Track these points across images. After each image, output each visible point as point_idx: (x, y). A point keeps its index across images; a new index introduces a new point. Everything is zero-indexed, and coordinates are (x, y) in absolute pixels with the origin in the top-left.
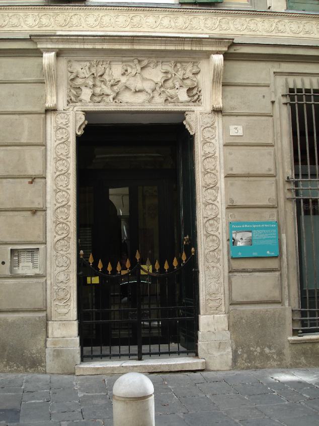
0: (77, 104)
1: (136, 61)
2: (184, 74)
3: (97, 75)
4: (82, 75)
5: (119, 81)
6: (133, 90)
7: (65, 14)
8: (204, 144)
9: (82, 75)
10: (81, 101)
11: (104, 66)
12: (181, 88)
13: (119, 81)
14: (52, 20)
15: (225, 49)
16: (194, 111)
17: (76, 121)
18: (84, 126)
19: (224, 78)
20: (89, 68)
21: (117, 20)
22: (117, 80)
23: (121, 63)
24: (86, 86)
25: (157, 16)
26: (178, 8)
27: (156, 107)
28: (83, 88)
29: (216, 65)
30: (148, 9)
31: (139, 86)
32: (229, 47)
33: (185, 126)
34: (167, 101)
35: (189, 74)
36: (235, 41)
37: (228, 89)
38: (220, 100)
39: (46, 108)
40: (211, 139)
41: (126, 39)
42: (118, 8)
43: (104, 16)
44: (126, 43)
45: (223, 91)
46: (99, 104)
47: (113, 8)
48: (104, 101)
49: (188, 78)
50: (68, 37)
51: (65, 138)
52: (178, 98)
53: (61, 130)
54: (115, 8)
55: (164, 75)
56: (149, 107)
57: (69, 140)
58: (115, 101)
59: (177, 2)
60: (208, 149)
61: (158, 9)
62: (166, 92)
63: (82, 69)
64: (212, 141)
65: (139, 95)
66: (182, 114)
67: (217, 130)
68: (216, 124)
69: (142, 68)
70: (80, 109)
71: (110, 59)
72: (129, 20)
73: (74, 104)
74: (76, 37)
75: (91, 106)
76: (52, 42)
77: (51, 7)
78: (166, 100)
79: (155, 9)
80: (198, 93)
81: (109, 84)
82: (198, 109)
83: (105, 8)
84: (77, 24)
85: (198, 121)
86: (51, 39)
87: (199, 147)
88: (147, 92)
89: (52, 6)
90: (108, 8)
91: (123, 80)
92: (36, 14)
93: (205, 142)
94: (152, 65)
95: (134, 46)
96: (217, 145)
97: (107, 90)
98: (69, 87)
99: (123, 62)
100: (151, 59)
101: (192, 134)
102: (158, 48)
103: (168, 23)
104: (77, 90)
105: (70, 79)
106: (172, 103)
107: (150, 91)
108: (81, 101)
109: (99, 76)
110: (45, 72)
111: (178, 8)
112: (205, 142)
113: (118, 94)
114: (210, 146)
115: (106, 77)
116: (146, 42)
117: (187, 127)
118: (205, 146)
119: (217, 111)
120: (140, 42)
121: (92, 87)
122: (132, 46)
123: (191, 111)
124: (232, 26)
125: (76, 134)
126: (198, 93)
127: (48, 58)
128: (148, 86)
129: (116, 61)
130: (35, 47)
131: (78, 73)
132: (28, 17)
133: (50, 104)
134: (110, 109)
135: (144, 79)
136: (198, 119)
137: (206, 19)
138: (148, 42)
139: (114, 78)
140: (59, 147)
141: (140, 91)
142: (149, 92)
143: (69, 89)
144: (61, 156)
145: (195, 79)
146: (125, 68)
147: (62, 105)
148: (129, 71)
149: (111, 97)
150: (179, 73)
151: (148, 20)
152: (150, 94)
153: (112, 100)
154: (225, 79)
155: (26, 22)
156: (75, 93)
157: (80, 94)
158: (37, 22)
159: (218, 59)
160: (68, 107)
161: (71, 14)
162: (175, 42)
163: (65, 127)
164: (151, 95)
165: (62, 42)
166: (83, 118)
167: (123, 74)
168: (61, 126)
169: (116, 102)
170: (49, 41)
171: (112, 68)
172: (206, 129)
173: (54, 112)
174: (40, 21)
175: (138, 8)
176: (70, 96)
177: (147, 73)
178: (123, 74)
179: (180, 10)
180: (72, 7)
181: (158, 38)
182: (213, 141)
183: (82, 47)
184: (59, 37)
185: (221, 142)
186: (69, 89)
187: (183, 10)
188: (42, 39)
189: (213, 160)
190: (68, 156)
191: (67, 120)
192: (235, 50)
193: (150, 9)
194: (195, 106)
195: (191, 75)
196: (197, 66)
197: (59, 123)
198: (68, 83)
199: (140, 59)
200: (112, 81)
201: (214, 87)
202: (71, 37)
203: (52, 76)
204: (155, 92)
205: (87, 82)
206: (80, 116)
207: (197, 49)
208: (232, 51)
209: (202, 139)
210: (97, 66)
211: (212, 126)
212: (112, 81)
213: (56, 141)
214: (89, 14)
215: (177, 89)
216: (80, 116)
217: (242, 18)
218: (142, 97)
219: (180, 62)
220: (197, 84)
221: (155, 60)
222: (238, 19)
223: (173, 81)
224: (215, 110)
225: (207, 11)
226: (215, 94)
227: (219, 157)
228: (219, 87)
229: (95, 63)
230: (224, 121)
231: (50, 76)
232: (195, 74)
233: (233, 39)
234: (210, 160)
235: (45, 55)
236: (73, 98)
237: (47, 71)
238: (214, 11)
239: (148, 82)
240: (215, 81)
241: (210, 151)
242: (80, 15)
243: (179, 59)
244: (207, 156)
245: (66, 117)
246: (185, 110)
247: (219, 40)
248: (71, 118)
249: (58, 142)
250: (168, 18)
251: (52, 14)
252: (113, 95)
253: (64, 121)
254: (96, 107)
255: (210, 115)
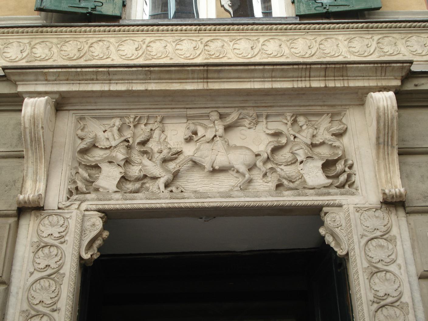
0: (87, 195)
1: (214, 116)
2: (314, 136)
3: (134, 142)
4: (104, 143)
5: (179, 153)
6: (208, 167)
7: (81, 40)
8: (373, 274)
9: (104, 143)
10: (97, 190)
11: (150, 127)
12: (309, 160)
13: (179, 153)
14: (55, 50)
15: (397, 83)
16: (340, 206)
17: (83, 232)
18: (99, 242)
19: (401, 140)
20: (119, 130)
21: (178, 47)
22: (174, 151)
23: (185, 121)
24: (110, 162)
25: (255, 38)
26: (295, 24)
27: (257, 199)
28: (106, 168)
29: (382, 109)
30: (236, 27)
31: (221, 160)
32: (404, 80)
33: (323, 238)
34: (281, 188)
35: (323, 134)
36: (414, 68)
37: (411, 159)
38: (398, 181)
39: (19, 203)
40: (388, 264)
41: (193, 71)
42: (179, 28)
43: (154, 42)
44: (193, 79)
45: (401, 164)
46: (136, 195)
47: (170, 27)
48: (147, 189)
49: (323, 144)
50: (79, 70)
51: (53, 265)
52: (305, 181)
53: (46, 250)
54: (175, 28)
55: (271, 139)
56: (243, 199)
57: (61, 271)
58: (169, 189)
59: (294, 16)
60: (382, 287)
61: (256, 27)
62: (278, 170)
63: (104, 132)
64: (392, 268)
65: (222, 177)
66: (315, 214)
67: (399, 243)
68: (394, 231)
69: (227, 128)
70: (94, 207)
71: (163, 112)
72: (201, 46)
73: (81, 196)
74: (95, 69)
75: (118, 200)
76: (46, 80)
77: (54, 29)
78: (279, 186)
79: (250, 27)
80: (347, 169)
81: (158, 157)
82: (349, 201)
83: (156, 28)
84: (101, 55)
85: (352, 225)
86: (46, 74)
87: (361, 282)
88: (238, 172)
89: (56, 26)
90: (161, 28)
91: (189, 150)
92: (26, 41)
93: (374, 271)
94: (246, 122)
95: (209, 84)
96: (404, 277)
97: (153, 168)
98: (77, 165)
99: (188, 118)
100: (245, 112)
101: (340, 252)
102: (257, 85)
103: (277, 48)
104: (93, 172)
105: (78, 149)
106: (292, 189)
107: (243, 169)
108: (97, 190)
109: (139, 144)
110: (25, 131)
111: (295, 24)
112: (374, 271)
113: (176, 175)
114: (387, 280)
115: (152, 145)
116: (233, 75)
117: (329, 239)
118: (376, 279)
119: (393, 203)
120: (221, 75)
121: (122, 163)
122: (205, 84)
123: (333, 206)
124: (403, 50)
125: (81, 258)
126: (347, 169)
127: (34, 107)
128: (238, 159)
129: (173, 117)
130: (13, 91)
131: (95, 138)
132: (9, 46)
133: (30, 192)
134: (158, 206)
135: (229, 147)
136: (353, 222)
137: (350, 40)
138: (236, 75)
139: (169, 146)
140: (37, 286)
141: (223, 170)
142: (241, 170)
143: (76, 168)
144: (40, 308)
145: (337, 144)
146: (192, 127)
147: (55, 197)
148: (200, 134)
149: (161, 183)
150: (304, 134)
151: (236, 46)
152: (244, 175)
153: (162, 187)
154: (403, 140)
155: (5, 54)
156: (86, 175)
157: (97, 178)
158: (25, 54)
159: (385, 100)
160: (68, 203)
161: (91, 41)
162: (291, 75)
163: (56, 243)
164: (247, 176)
165: (67, 80)
166: (99, 224)
167: (189, 140)
168: (49, 241)
169: (171, 191)
170: (41, 78)
171: (166, 129)
172: (374, 242)
173: (38, 213)
174: (32, 52)
175: (218, 27)
176: (75, 182)
177: (236, 137)
178: (189, 140)
179: (299, 26)
180: (93, 28)
181: (257, 67)
182: (392, 268)
183: (106, 88)
184: (60, 70)
185: (412, 270)
186: (76, 168)
187: (303, 26)
188: (27, 73)
189: (398, 312)
190: (54, 307)
191: (62, 229)
192: (416, 85)
193: (241, 27)
194: (342, 194)
195: (328, 136)
196: (340, 121)
197: (45, 235)
198: (74, 158)
199: (222, 111)
200: (165, 152)
201: (381, 155)
202: (84, 70)
203: (39, 140)
204: (255, 172)
205: (114, 154)
206: (93, 220)
207: (339, 84)
208: (410, 86)
209: (366, 265)
210: (135, 126)
211: (386, 235)
212: (165, 152)
213: (32, 274)
214: (125, 39)
215: (302, 162)
216: (93, 220)
217: (423, 35)
218: (225, 182)
219: (305, 115)
220: (344, 151)
221: (251, 112)
222: (414, 38)
223: (291, 149)
224: (389, 200)
225: (351, 25)
226: (385, 167)
227: (410, 304)
228: (392, 153)
229: (132, 120)
230: (412, 223)
231: (35, 140)
232: (339, 135)
233: (411, 62)
234: (391, 311)
235: (27, 101)
236: (80, 184)
237: (28, 131)
238: (365, 25)
239: (238, 152)
240: (382, 141)
241: (389, 291)
242: (108, 41)
243: (303, 110)
244: (383, 303)
245: (61, 222)
246: (321, 203)
247: (382, 67)
248: (73, 224)
249: (37, 275)
250: (276, 41)
251: (55, 41)
252: (165, 177)
253: (55, 231)
254: (128, 202)
255: (379, 213)
